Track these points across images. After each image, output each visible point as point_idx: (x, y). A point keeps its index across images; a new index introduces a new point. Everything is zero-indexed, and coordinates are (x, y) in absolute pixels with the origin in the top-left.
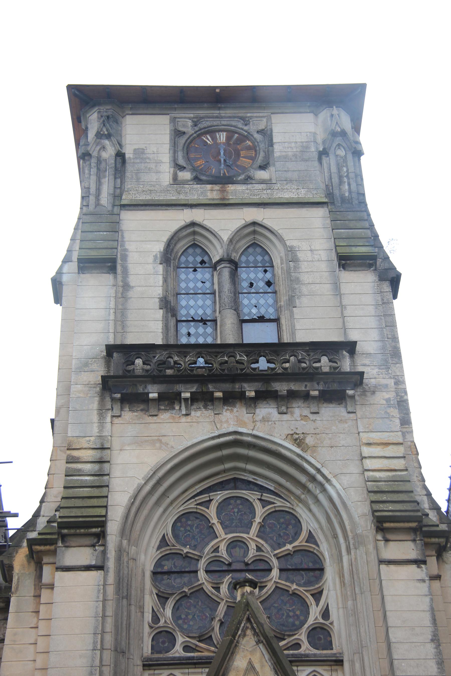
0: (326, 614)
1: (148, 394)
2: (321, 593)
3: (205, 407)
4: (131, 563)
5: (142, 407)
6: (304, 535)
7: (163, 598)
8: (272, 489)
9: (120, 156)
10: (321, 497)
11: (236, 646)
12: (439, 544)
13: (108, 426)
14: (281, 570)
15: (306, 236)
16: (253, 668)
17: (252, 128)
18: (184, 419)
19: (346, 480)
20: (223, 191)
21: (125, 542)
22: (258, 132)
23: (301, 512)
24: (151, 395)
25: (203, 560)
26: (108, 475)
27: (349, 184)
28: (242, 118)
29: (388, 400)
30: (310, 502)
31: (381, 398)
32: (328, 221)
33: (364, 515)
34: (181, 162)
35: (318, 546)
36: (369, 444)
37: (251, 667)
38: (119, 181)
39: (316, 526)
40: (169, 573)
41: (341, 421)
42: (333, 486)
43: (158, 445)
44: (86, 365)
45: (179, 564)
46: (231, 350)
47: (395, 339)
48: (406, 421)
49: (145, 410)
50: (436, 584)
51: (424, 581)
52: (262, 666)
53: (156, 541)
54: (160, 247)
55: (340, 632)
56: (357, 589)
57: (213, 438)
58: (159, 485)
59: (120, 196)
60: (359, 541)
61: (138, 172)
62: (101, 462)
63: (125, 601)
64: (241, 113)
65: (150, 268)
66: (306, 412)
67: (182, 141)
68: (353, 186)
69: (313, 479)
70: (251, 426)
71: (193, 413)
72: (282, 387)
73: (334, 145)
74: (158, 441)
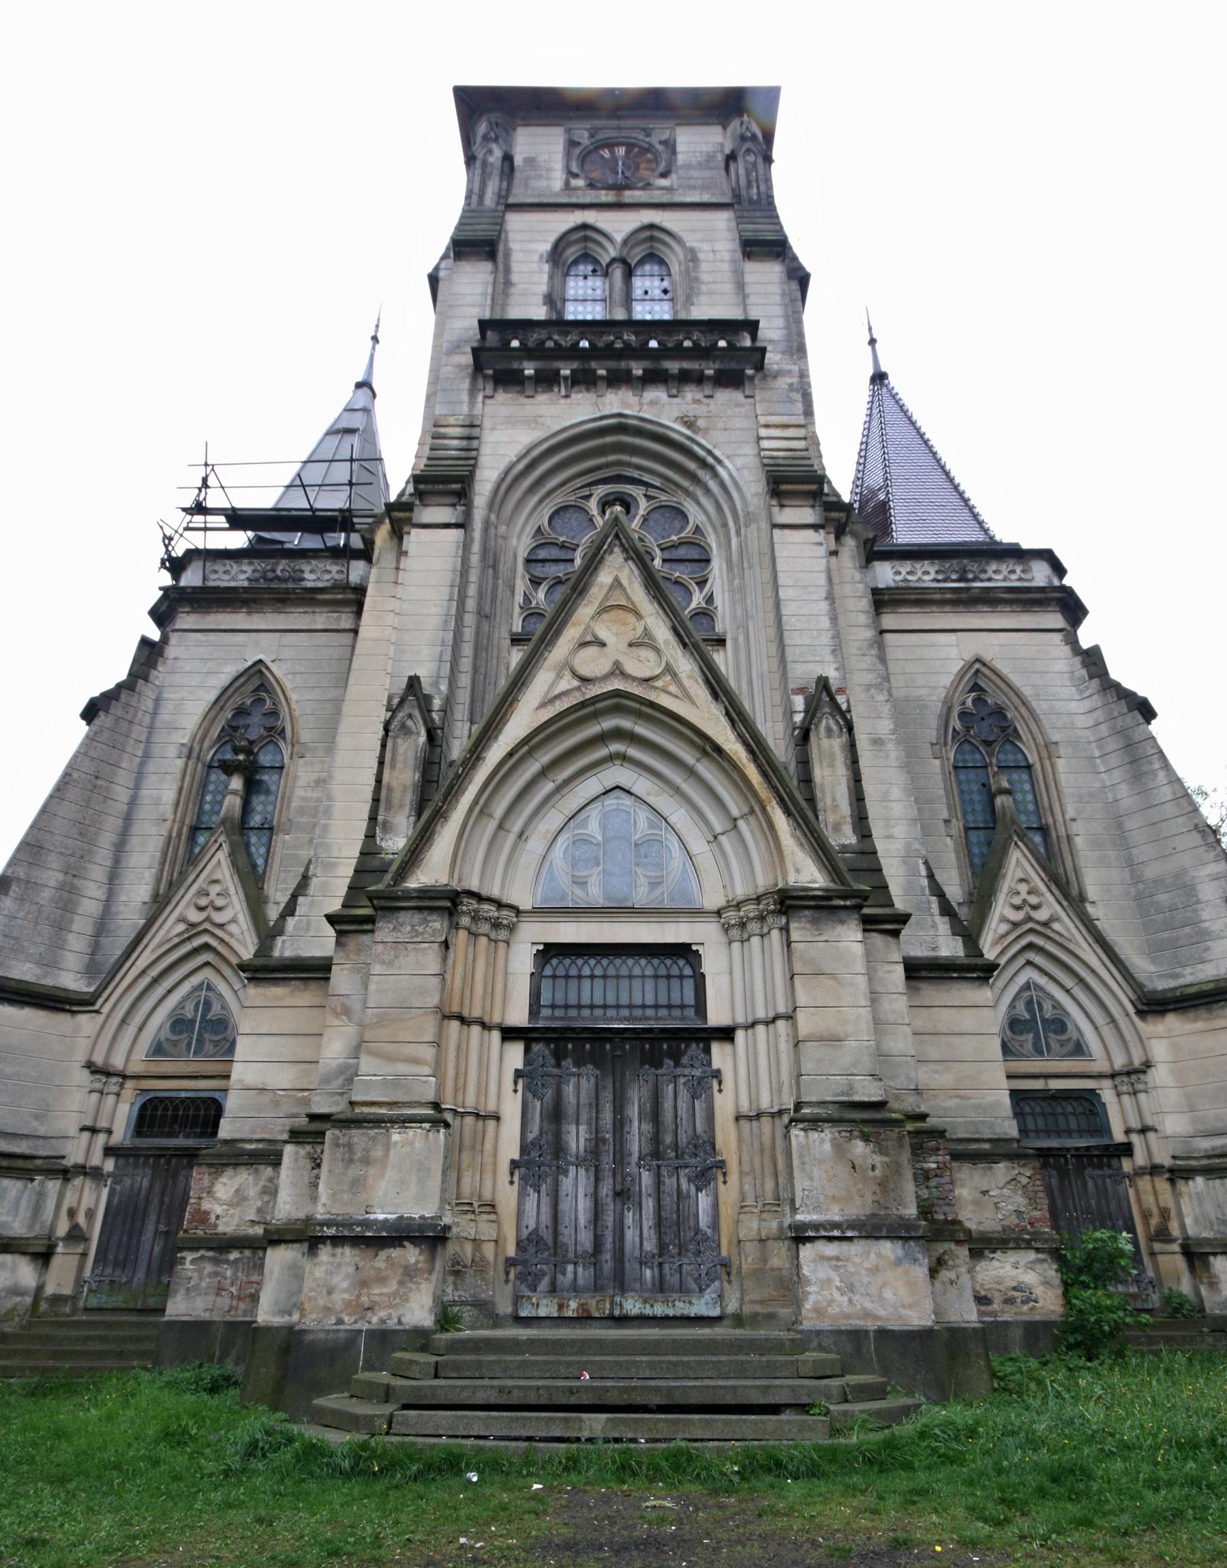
0: (710, 599)
1: (522, 371)
2: (705, 581)
3: (588, 390)
4: (500, 541)
5: (518, 388)
6: (690, 527)
7: (536, 582)
8: (658, 484)
9: (508, 158)
10: (712, 485)
11: (600, 562)
12: (838, 520)
13: (479, 405)
14: (664, 561)
15: (710, 237)
16: (620, 584)
17: (654, 140)
18: (563, 401)
19: (739, 461)
20: (618, 195)
21: (493, 517)
22: (660, 143)
23: (690, 508)
24: (527, 372)
25: (580, 549)
26: (477, 449)
27: (758, 187)
28: (643, 129)
29: (791, 385)
30: (699, 493)
31: (782, 383)
32: (734, 224)
33: (757, 494)
34: (575, 169)
35: (703, 535)
36: (767, 426)
37: (617, 583)
38: (505, 184)
39: (704, 518)
40: (543, 561)
41: (737, 405)
42: (725, 467)
43: (533, 425)
44: (458, 347)
45: (555, 553)
46: (618, 329)
47: (801, 334)
48: (808, 412)
49: (522, 392)
50: (833, 559)
51: (821, 544)
52: (630, 583)
53: (530, 530)
54: (547, 247)
55: (724, 616)
56: (745, 565)
57: (594, 420)
58: (531, 470)
59: (507, 197)
60: (750, 518)
61: (527, 179)
62: (469, 438)
63: (490, 571)
64: (642, 123)
65: (535, 267)
66: (699, 396)
67: (577, 151)
68: (763, 188)
69: (703, 464)
70: (637, 408)
71: (573, 396)
72: (673, 366)
73: (744, 149)
74: (535, 421)
